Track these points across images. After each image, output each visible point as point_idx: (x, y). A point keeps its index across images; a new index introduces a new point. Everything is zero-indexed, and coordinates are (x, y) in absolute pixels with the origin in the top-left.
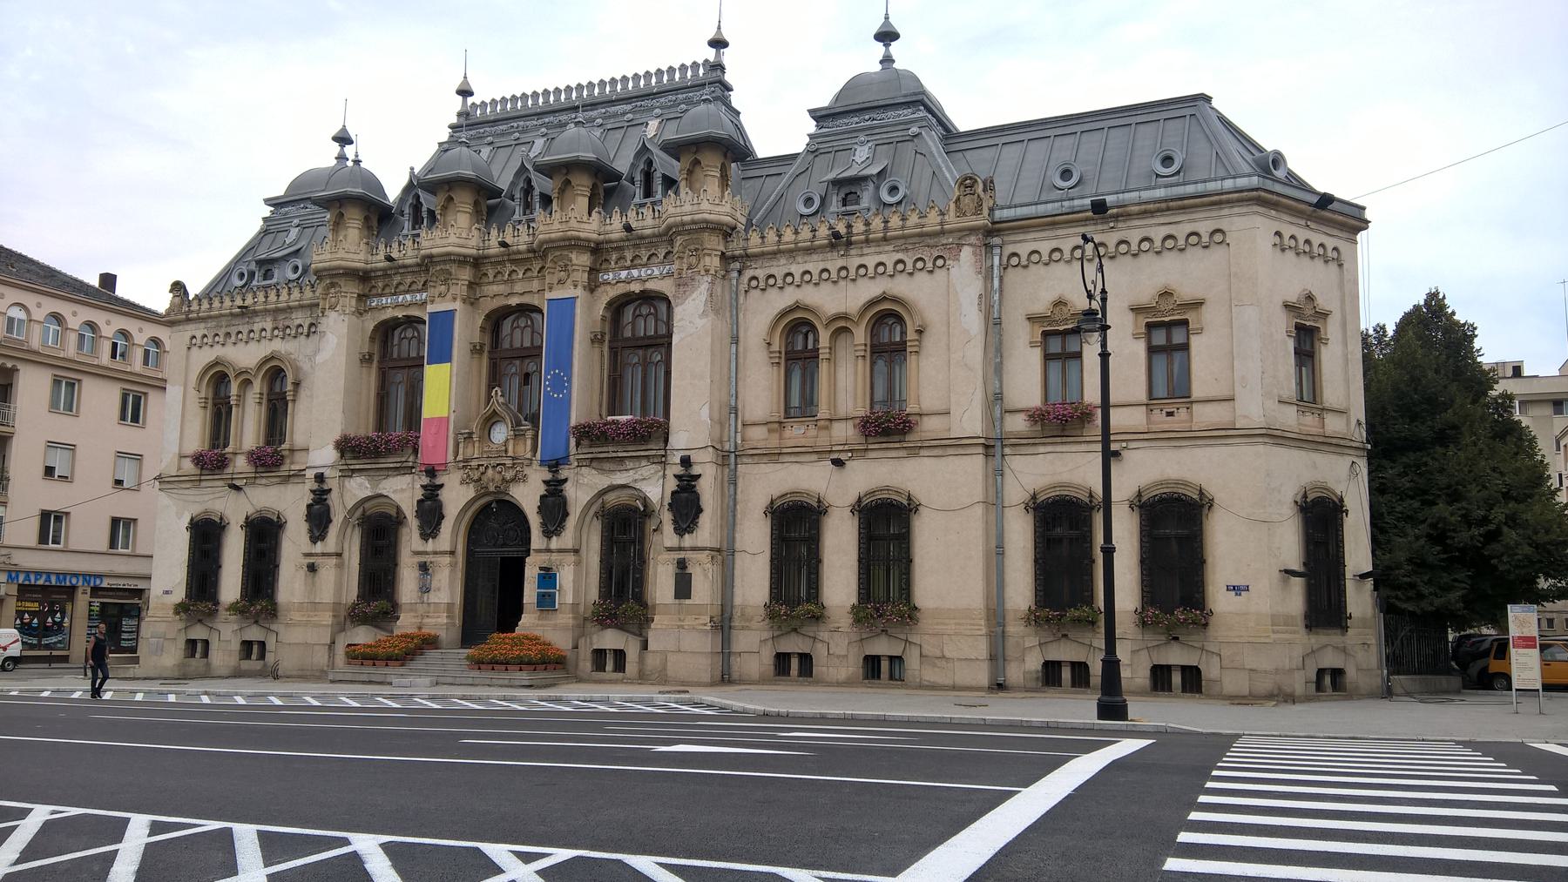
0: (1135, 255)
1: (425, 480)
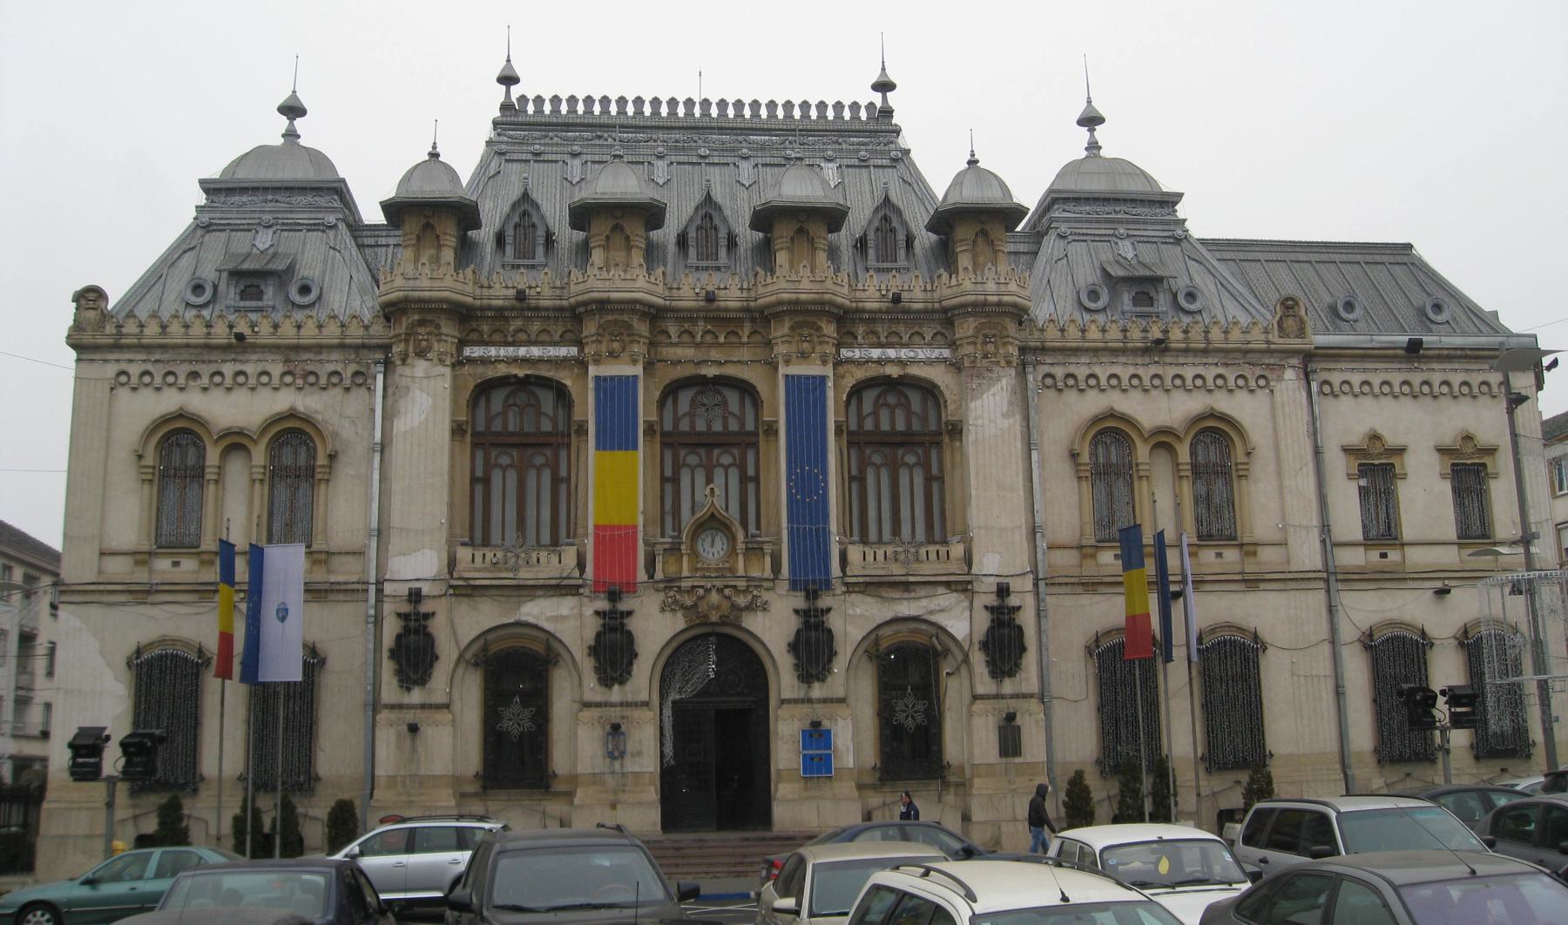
0: (253, 389)
1: (603, 604)
